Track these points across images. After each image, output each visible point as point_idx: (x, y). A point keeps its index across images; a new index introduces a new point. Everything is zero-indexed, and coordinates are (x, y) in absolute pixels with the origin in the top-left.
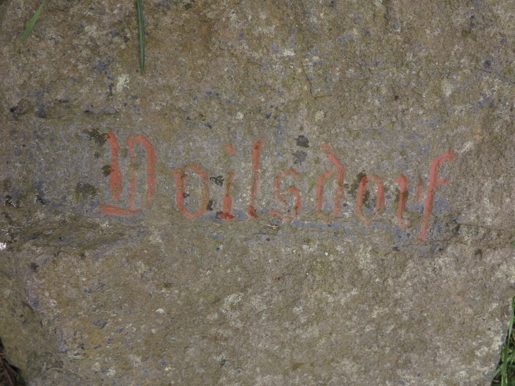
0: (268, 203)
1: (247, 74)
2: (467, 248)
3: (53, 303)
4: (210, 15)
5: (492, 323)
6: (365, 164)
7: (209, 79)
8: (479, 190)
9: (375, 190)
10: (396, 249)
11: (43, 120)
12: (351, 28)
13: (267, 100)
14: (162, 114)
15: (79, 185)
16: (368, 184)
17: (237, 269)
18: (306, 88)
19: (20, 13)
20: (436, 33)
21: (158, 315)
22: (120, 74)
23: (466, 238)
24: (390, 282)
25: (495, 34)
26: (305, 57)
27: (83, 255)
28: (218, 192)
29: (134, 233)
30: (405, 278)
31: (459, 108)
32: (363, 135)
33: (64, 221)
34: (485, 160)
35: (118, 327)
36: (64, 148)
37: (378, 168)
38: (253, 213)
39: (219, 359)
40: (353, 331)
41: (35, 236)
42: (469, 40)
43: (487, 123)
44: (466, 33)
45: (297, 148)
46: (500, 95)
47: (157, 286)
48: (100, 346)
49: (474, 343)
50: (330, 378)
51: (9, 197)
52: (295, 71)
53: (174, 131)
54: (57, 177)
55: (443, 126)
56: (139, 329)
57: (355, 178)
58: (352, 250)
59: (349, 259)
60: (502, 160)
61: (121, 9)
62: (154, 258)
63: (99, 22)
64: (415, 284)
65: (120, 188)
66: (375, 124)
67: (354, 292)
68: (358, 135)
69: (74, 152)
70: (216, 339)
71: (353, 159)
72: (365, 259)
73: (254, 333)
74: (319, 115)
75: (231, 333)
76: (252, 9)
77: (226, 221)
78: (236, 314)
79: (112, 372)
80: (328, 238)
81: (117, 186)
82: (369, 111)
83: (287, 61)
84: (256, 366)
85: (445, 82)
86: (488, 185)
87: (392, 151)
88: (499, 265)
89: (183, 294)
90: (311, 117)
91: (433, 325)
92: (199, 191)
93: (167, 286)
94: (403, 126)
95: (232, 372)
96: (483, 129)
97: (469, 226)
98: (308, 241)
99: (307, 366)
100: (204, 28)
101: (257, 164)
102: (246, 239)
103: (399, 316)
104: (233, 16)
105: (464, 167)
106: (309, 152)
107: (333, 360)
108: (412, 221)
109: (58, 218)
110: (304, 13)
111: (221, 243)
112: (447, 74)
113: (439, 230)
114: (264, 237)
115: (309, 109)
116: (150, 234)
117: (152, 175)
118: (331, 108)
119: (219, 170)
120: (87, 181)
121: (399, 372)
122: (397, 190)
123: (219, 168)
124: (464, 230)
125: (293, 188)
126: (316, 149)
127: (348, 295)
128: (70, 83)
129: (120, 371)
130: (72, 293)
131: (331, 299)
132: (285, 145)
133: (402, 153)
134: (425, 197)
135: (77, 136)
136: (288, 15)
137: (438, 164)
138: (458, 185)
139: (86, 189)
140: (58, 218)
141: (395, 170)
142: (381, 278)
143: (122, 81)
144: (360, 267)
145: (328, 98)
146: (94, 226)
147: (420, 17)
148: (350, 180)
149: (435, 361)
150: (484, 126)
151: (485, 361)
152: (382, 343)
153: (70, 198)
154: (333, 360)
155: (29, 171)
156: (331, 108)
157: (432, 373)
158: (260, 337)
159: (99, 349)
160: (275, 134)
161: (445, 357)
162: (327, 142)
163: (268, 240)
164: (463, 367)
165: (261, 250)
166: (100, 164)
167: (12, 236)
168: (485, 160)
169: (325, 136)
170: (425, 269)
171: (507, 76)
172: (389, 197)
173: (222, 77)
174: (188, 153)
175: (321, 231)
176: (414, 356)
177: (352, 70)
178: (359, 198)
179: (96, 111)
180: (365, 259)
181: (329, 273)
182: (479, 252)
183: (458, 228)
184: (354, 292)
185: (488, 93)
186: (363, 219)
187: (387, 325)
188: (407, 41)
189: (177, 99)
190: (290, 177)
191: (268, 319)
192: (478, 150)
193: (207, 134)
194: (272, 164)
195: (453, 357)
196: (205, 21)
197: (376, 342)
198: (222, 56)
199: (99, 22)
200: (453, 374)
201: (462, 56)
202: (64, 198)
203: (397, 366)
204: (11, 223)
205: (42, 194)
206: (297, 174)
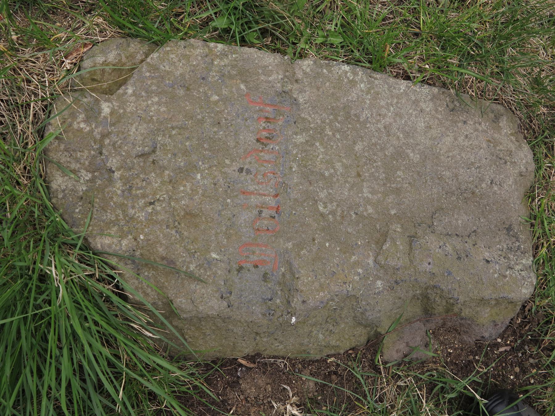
0: (272, 188)
1: (209, 197)
2: (294, 87)
3: (322, 294)
4: (182, 214)
5: (334, 72)
6: (252, 139)
7: (212, 215)
8: (266, 82)
9: (265, 134)
10: (295, 123)
11: (233, 294)
12: (186, 146)
13: (221, 187)
14: (228, 238)
15: (263, 280)
16: (262, 137)
17: (305, 204)
18: (214, 168)
19: (184, 301)
20: (188, 104)
21: (330, 246)
22: (211, 256)
23: (289, 88)
24: (312, 126)
25: (189, 75)
26: (200, 169)
27: (298, 278)
28: (266, 213)
29: (287, 256)
30: (115, 345)
31: (224, 92)
32: (237, 140)
33: (281, 290)
34: (250, 79)
35: (336, 266)
36: (246, 285)
37: (254, 132)
38: (276, 196)
39: (354, 216)
40: (339, 144)
41: (289, 302)
42: (191, 87)
43: (231, 77)
44: (188, 89)
45: (244, 173)
46: (218, 72)
47: (314, 245)
48: (345, 275)
49: (345, 81)
50: (366, 156)
51: (269, 314)
52: (207, 173)
53: (236, 233)
54: (259, 290)
55: (232, 99)
56: (337, 256)
57: (259, 144)
58: (296, 145)
59: (300, 147)
60: (250, 71)
61: (183, 253)
62: (299, 246)
63: (189, 263)
64: (313, 113)
65: (264, 261)
66: (232, 134)
67: (318, 144)
68: (237, 142)
69: (247, 281)
70: (343, 217)
71: (249, 145)
72: (300, 139)
73: (339, 196)
74: (227, 162)
75: (339, 209)
76: (179, 193)
77: (281, 209)
78: (329, 206)
79: (360, 271)
80: (289, 158)
81: (263, 262)
82: (226, 137)
83: (203, 178)
84: (358, 196)
85: (211, 99)
86: (262, 78)
87: (245, 125)
88: (303, 70)
89: (318, 232)
90: (229, 166)
91: (335, 103)
92: (266, 222)
93: (314, 240)
94: (233, 120)
95: (361, 209)
96: (234, 79)
97: (283, 86)
98: (291, 168)
99: (359, 169)
100: (188, 217)
101: (252, 193)
102: (290, 200)
103: (330, 120)
104: (183, 202)
105: (253, 89)
106: (246, 167)
107: (356, 155)
108: (281, 114)
109: (279, 293)
110: (179, 169)
111: (292, 212)
112: (207, 97)
113: (284, 101)
114: (289, 190)
115: (225, 167)
116: (287, 248)
117: (258, 245)
118: (223, 156)
119: (255, 212)
120: (261, 276)
121: (361, 120)
122: (264, 122)
123: (254, 212)
124: (286, 89)
125: (264, 175)
126: (244, 164)
127: (319, 147)
128: (216, 279)
129: (359, 266)
130: (316, 284)
131: (321, 156)
132: (243, 179)
133: (247, 120)
134: (268, 108)
135: (240, 279)
136: (181, 176)
137: (252, 102)
138: (263, 92)
139: (265, 277)
140: (279, 293)
141: (255, 123)
142: (310, 131)
143: (214, 255)
144: (304, 141)
145: (219, 157)
146: (284, 275)
147: (180, 112)
148: (259, 146)
149: (355, 101)
150: (233, 79)
151: (355, 74)
152: (346, 129)
153: (269, 286)
154: (356, 155)
155: (257, 303)
156: (223, 156)
157: (361, 103)
158: (341, 193)
159: (347, 276)
160: (237, 184)
161: (354, 95)
162: (240, 158)
163: (290, 188)
164: (358, 86)
165: (295, 192)
166: (253, 269)
167: (289, 313)
168: (250, 79)
169: (238, 159)
170: (305, 108)
171: (209, 69)
172: (268, 127)
173: (211, 209)
174: (247, 227)
175: (285, 161)
176: (353, 112)
177: (205, 145)
178: (269, 141)
179: (229, 268)
180: (300, 139)
181: (308, 157)
182: (297, 81)
183: (284, 92)
184: (318, 144)
185: (217, 78)
186: (279, 139)
187: (336, 126)
188: (192, 118)
189: (221, 231)
190: (259, 177)
191: (332, 189)
192: (245, 82)
193: (238, 217)
194: (252, 185)
195: (353, 92)
196: (184, 216)
197: (345, 132)
198: (201, 208)
199: (189, 263)
200: (362, 91)
201: (199, 91)
202: (270, 288)
203: (358, 121)
204: (282, 315)
205: (267, 299)
206: (257, 173)
